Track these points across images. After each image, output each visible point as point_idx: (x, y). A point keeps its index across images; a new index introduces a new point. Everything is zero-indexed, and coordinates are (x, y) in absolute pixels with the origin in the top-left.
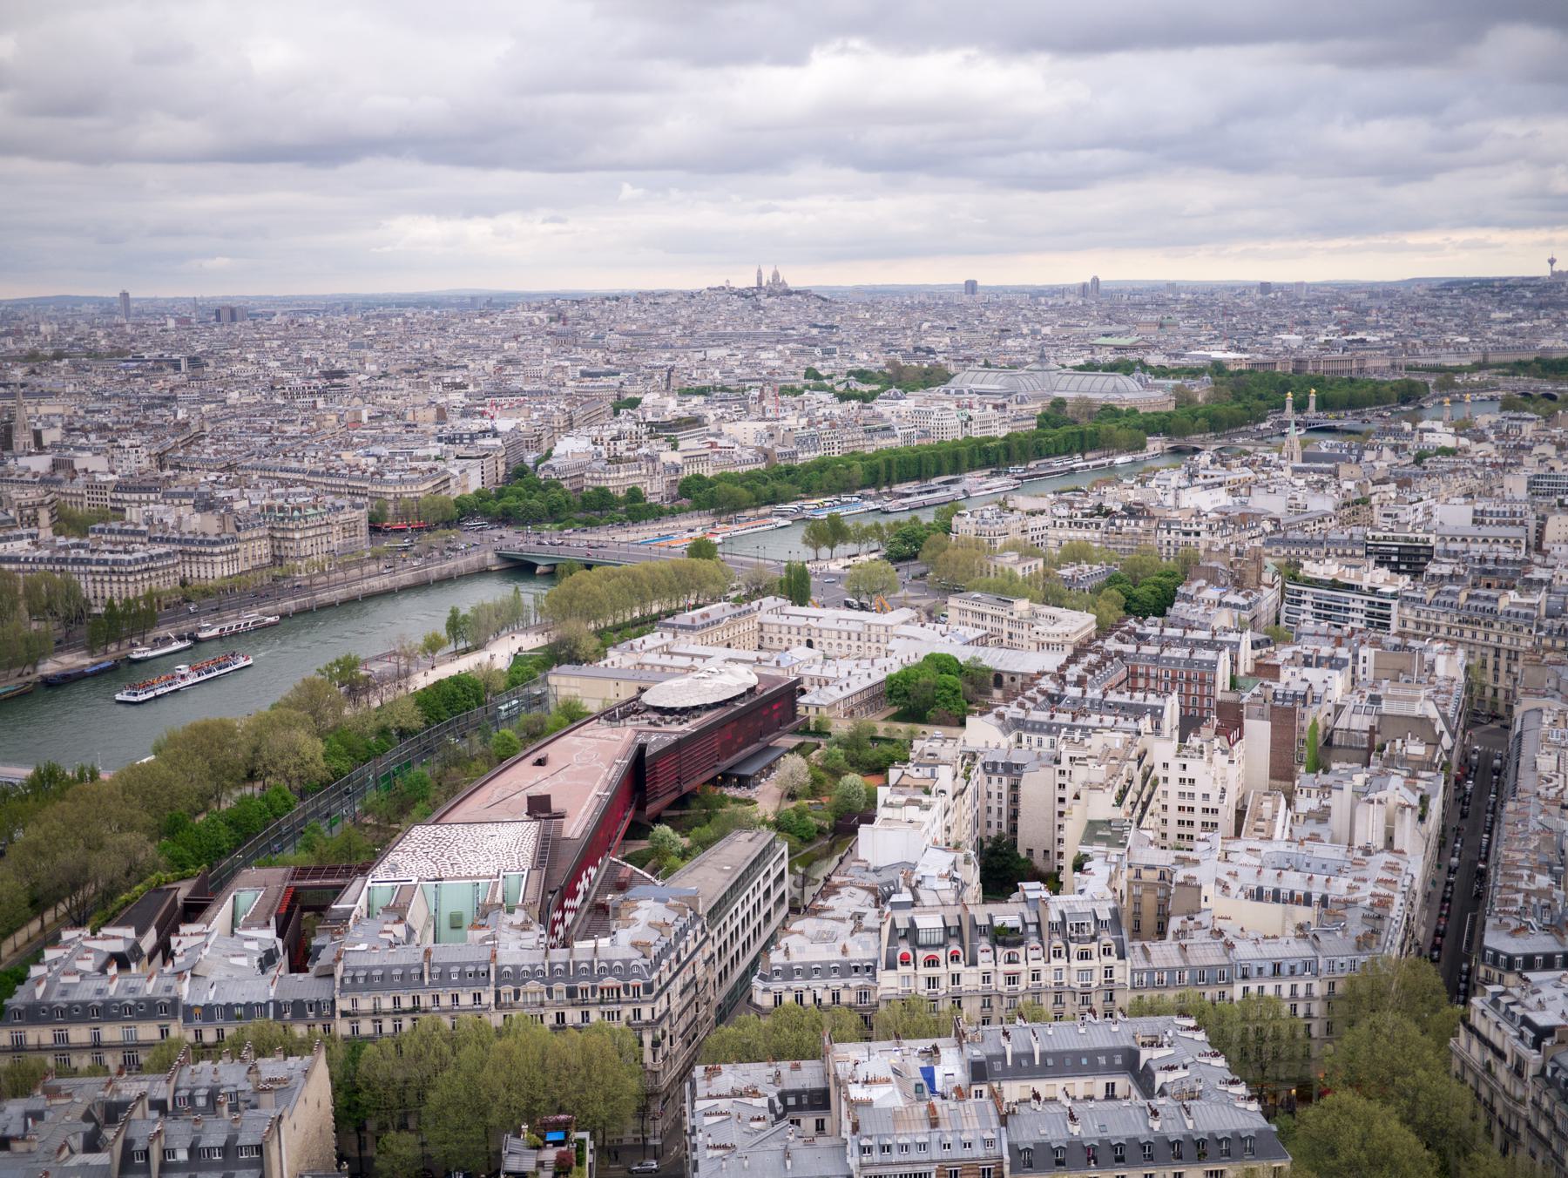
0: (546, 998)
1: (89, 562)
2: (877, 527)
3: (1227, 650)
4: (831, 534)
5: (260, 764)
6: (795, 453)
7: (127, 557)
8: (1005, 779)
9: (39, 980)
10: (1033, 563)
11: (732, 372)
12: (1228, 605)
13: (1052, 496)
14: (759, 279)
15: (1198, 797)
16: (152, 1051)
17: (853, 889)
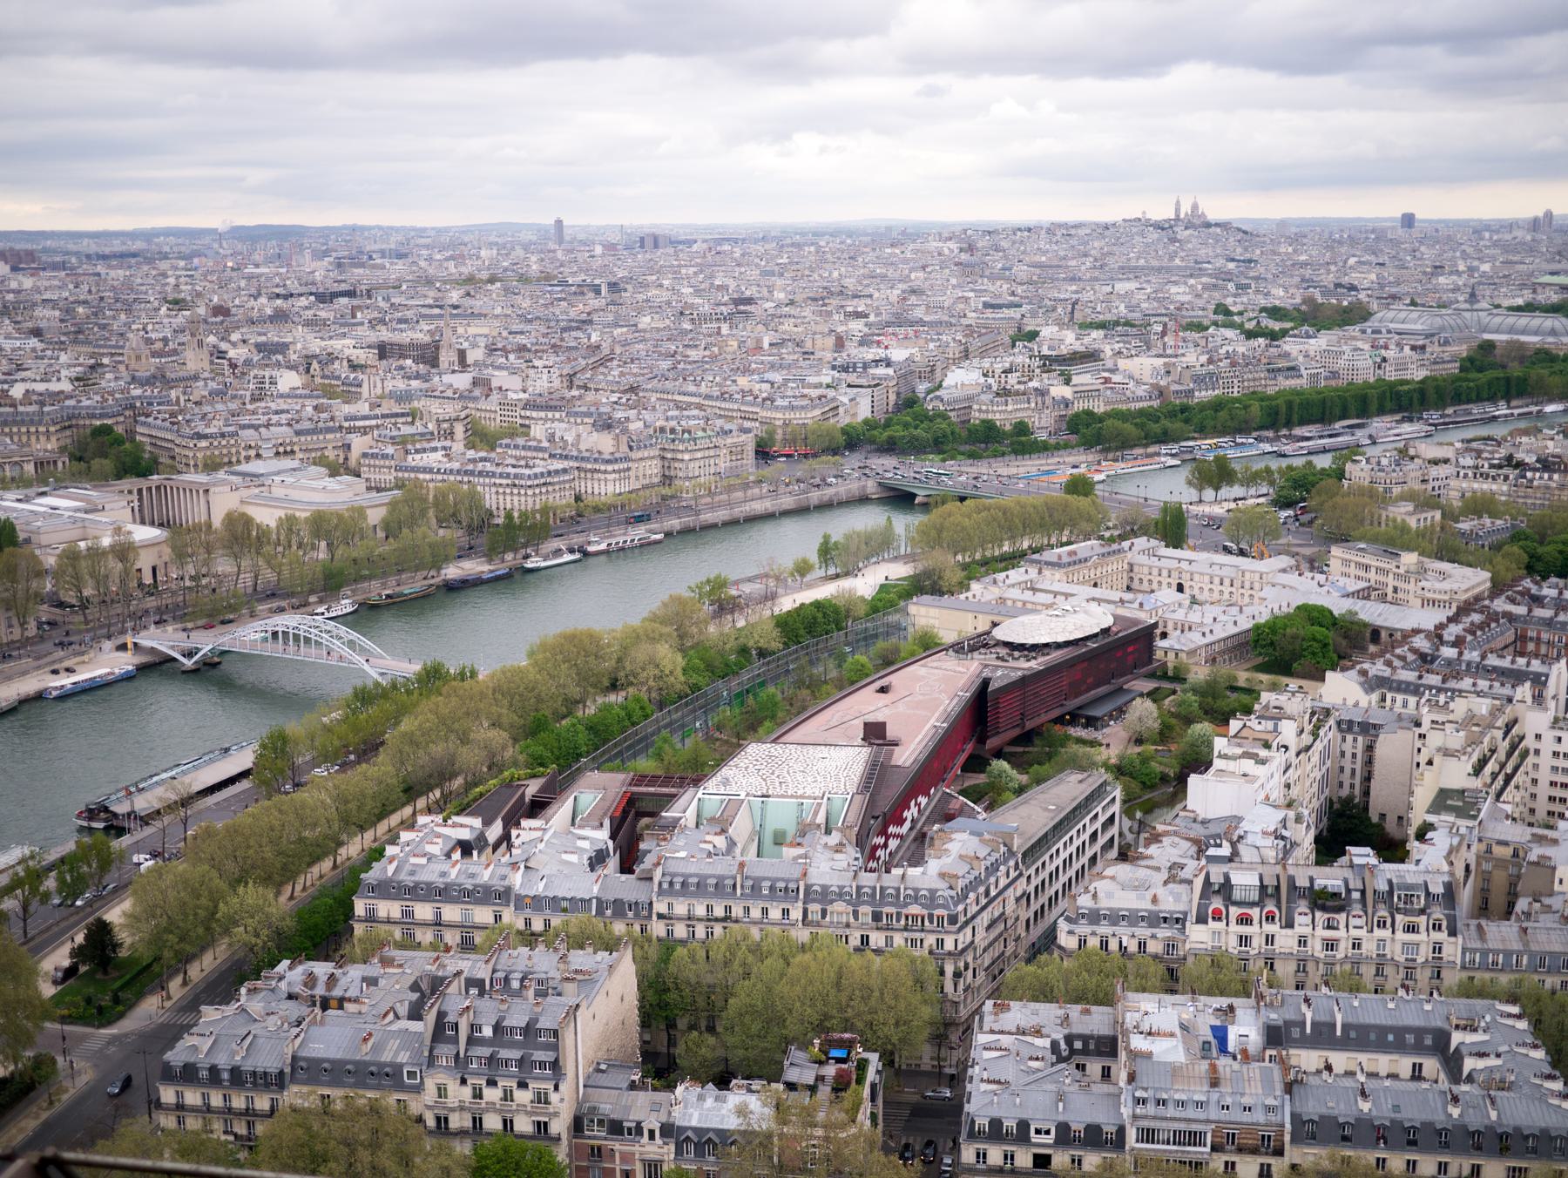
1: (494, 475)
2: (1268, 470)
4: (1216, 475)
5: (622, 674)
7: (527, 472)
8: (1360, 739)
10: (1429, 515)
13: (1459, 445)
14: (1177, 210)
17: (1177, 840)
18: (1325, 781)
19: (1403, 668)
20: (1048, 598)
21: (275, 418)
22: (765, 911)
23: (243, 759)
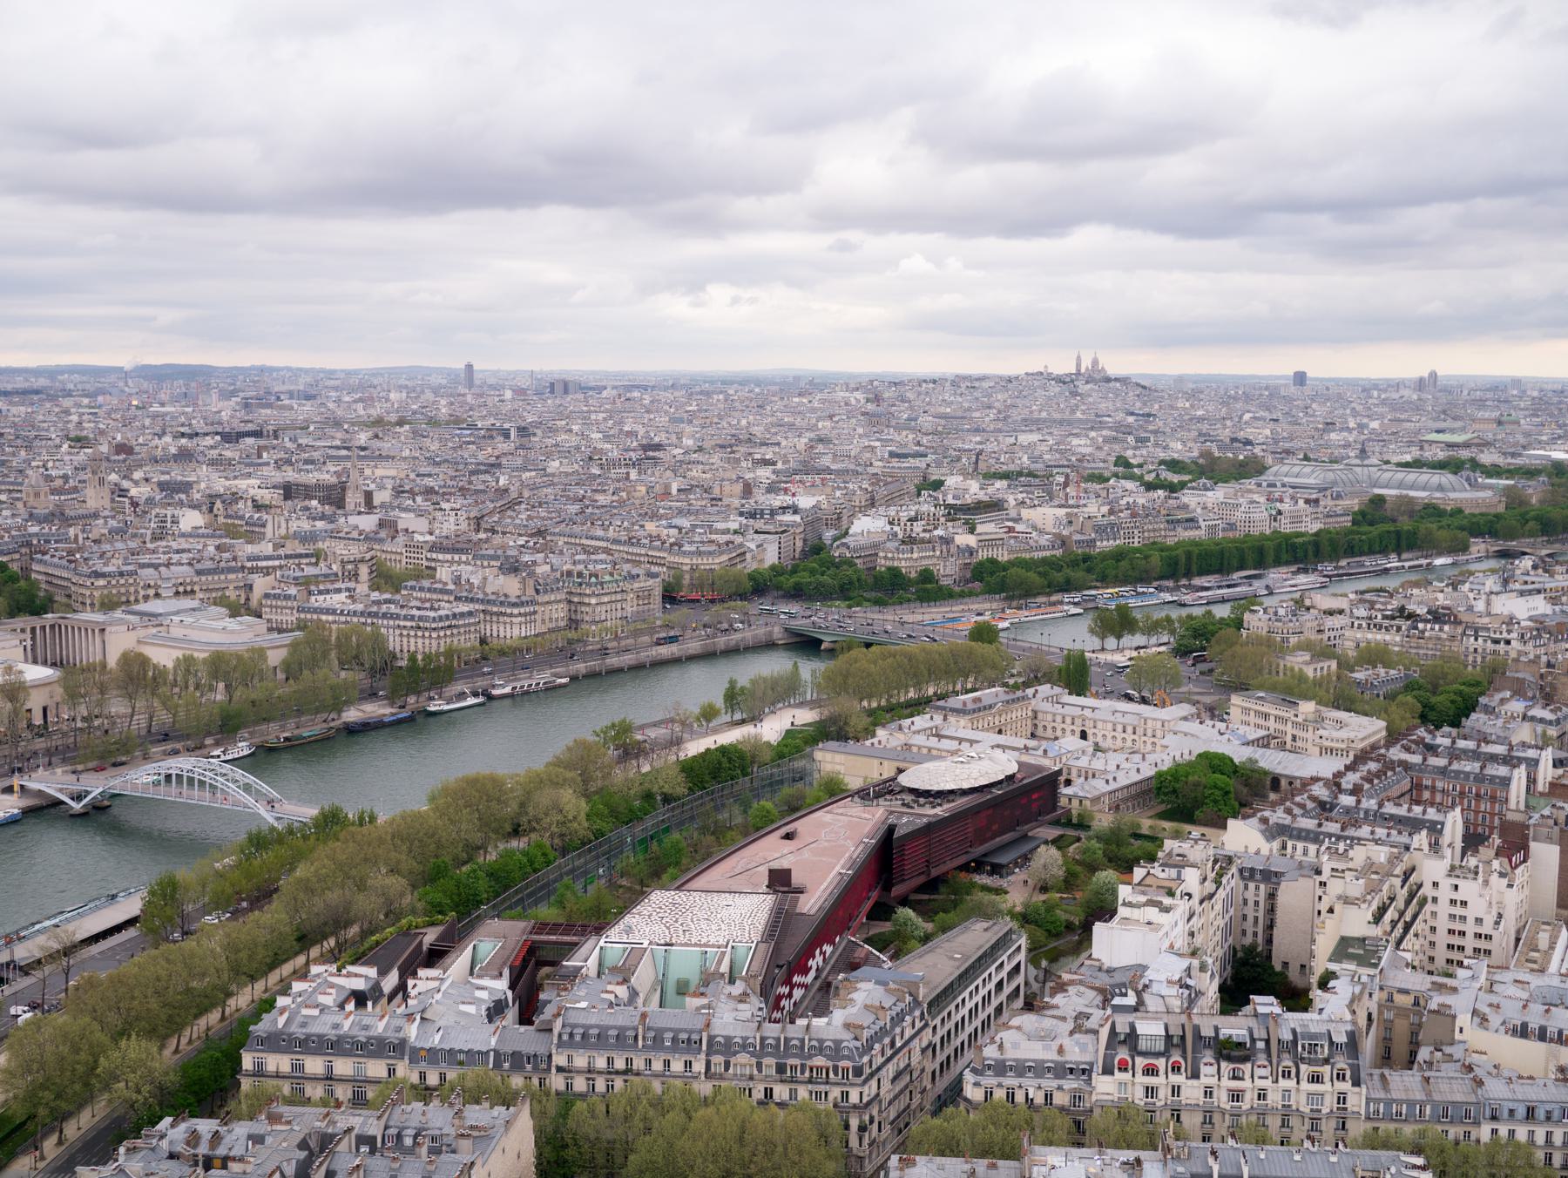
0: (755, 1072)
1: (398, 617)
2: (1168, 620)
3: (1523, 767)
4: (1117, 624)
6: (1093, 541)
7: (432, 614)
8: (1262, 887)
9: (283, 1011)
10: (1325, 665)
11: (1041, 457)
12: (1533, 719)
13: (1352, 596)
15: (1470, 920)
16: (377, 1088)
17: (1082, 989)
18: (1228, 930)
19: (1303, 816)
20: (953, 745)
21: (176, 557)
22: (667, 1063)
23: (130, 906)
